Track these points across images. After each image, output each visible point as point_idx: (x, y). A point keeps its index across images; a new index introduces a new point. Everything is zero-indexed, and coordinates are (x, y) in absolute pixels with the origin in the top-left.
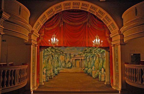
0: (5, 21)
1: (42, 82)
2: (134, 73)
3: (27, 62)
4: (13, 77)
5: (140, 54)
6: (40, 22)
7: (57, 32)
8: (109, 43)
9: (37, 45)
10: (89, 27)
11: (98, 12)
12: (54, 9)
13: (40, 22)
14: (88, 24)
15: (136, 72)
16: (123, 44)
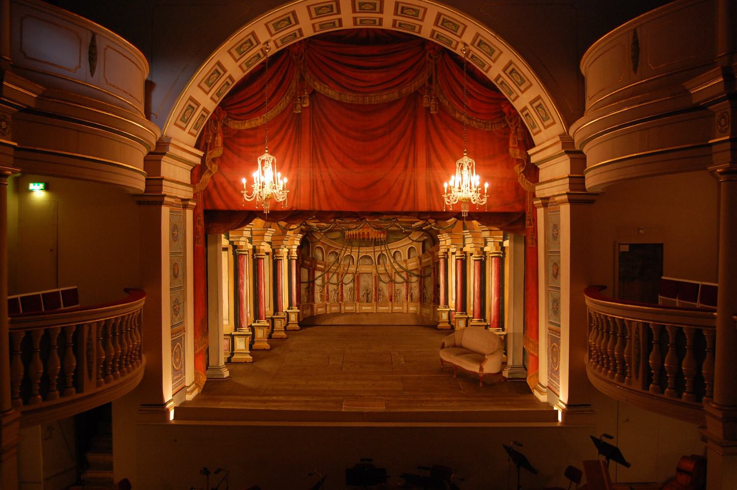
0: (22, 110)
1: (222, 362)
2: (615, 343)
3: (143, 279)
4: (74, 359)
5: (661, 245)
6: (201, 94)
7: (289, 139)
8: (525, 192)
9: (190, 203)
10: (432, 115)
11: (472, 44)
12: (263, 35)
13: (201, 94)
14: (425, 101)
15: (623, 336)
16: (580, 198)
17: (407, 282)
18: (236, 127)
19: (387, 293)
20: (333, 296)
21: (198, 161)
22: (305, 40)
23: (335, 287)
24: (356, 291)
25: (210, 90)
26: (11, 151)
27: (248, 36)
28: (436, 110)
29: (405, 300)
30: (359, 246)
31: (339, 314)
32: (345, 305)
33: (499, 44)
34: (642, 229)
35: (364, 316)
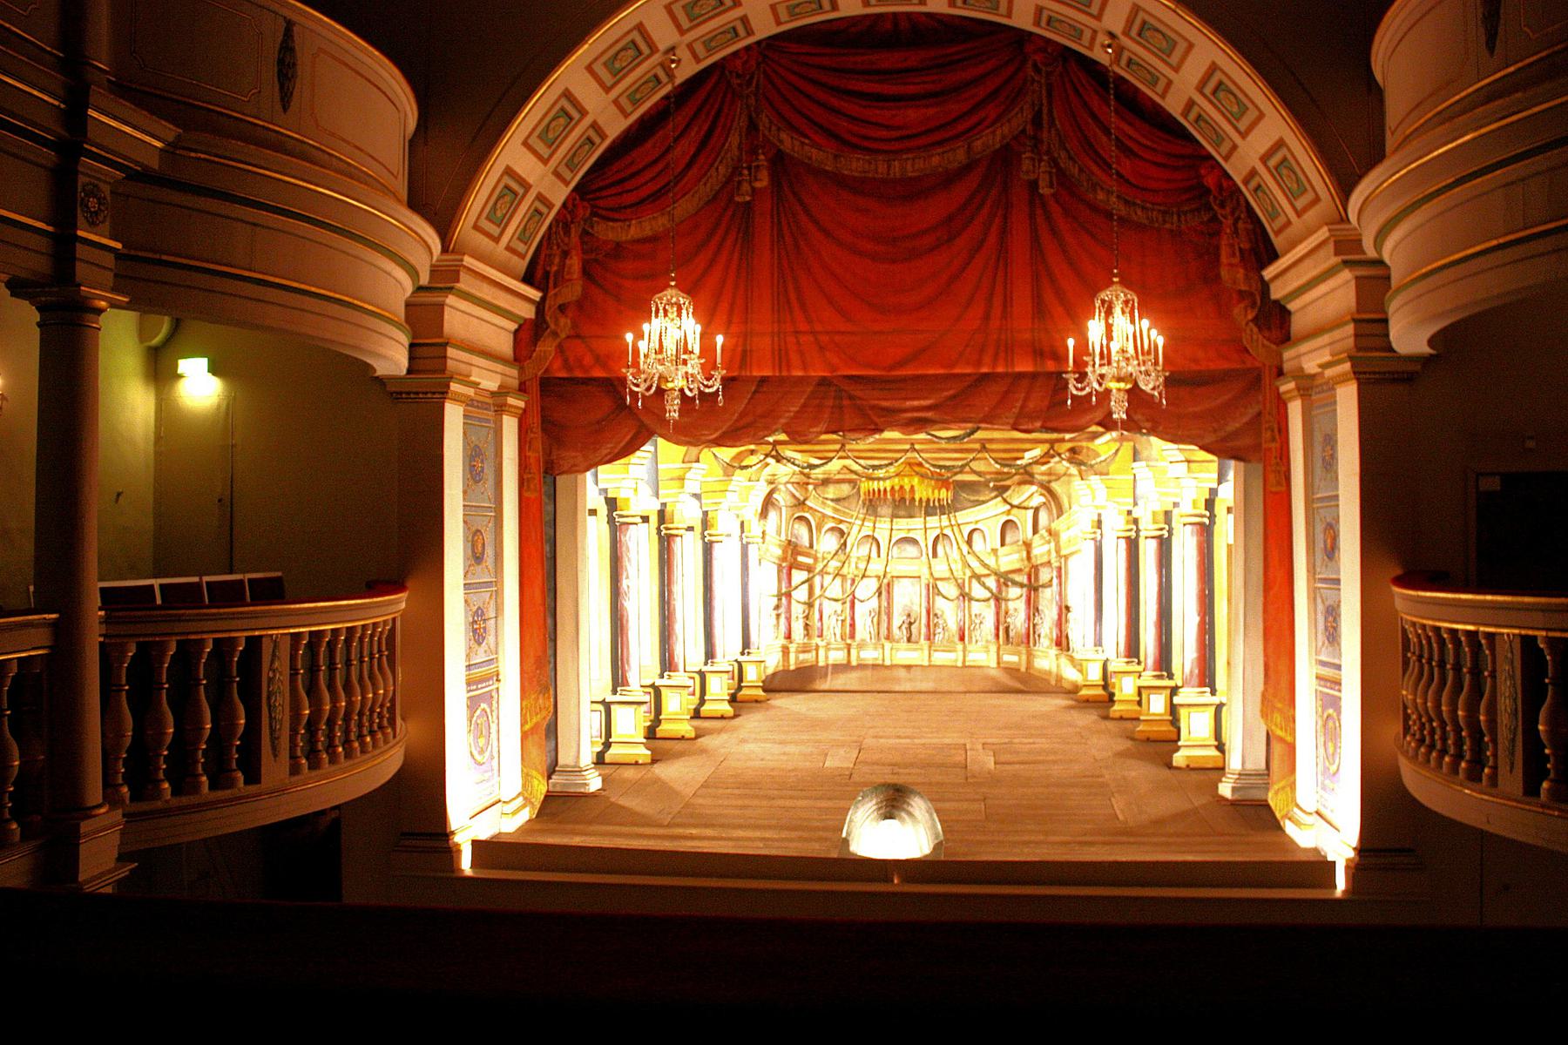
1: (587, 759)
11: (1126, 33)
14: (1026, 164)
17: (998, 599)
18: (611, 236)
19: (953, 628)
20: (833, 627)
21: (528, 312)
22: (759, 43)
23: (838, 606)
24: (884, 617)
25: (551, 156)
26: (109, 260)
27: (628, 32)
28: (1051, 186)
29: (991, 637)
30: (894, 516)
31: (845, 667)
32: (860, 647)
33: (1186, 26)
34: (1531, 438)
35: (902, 673)
